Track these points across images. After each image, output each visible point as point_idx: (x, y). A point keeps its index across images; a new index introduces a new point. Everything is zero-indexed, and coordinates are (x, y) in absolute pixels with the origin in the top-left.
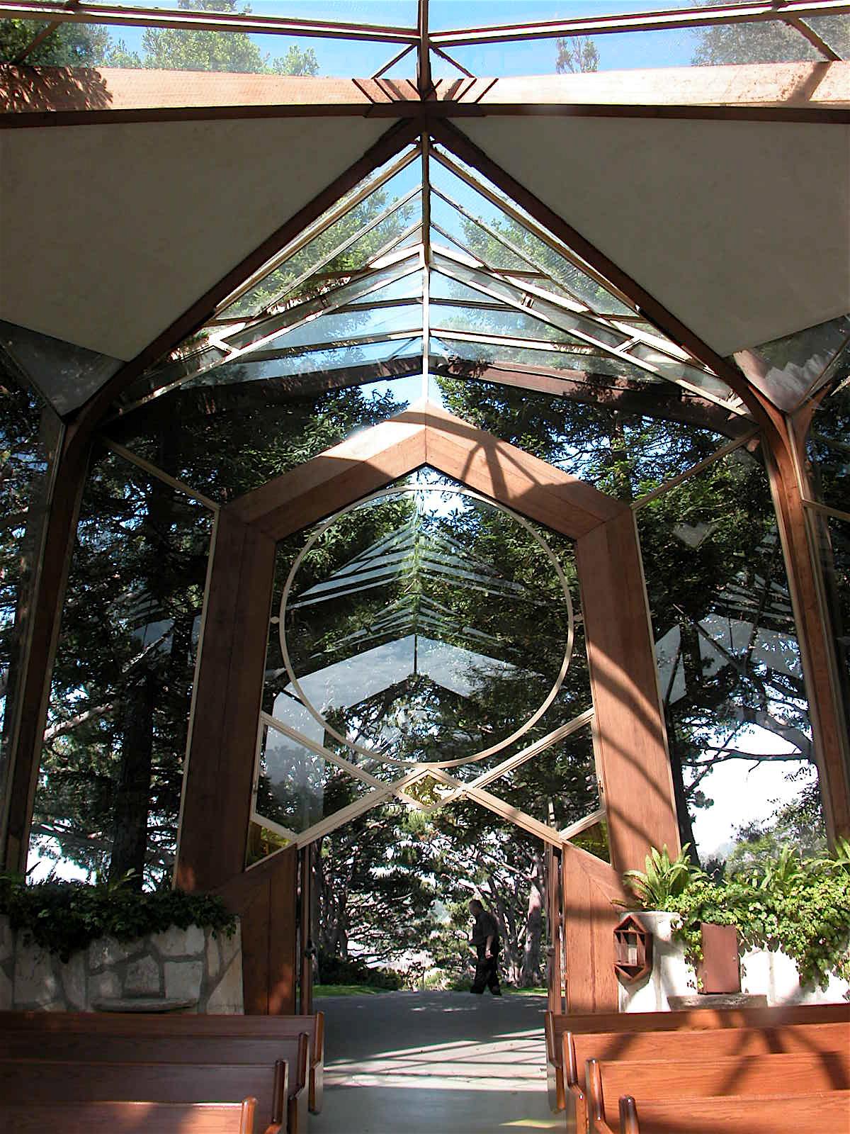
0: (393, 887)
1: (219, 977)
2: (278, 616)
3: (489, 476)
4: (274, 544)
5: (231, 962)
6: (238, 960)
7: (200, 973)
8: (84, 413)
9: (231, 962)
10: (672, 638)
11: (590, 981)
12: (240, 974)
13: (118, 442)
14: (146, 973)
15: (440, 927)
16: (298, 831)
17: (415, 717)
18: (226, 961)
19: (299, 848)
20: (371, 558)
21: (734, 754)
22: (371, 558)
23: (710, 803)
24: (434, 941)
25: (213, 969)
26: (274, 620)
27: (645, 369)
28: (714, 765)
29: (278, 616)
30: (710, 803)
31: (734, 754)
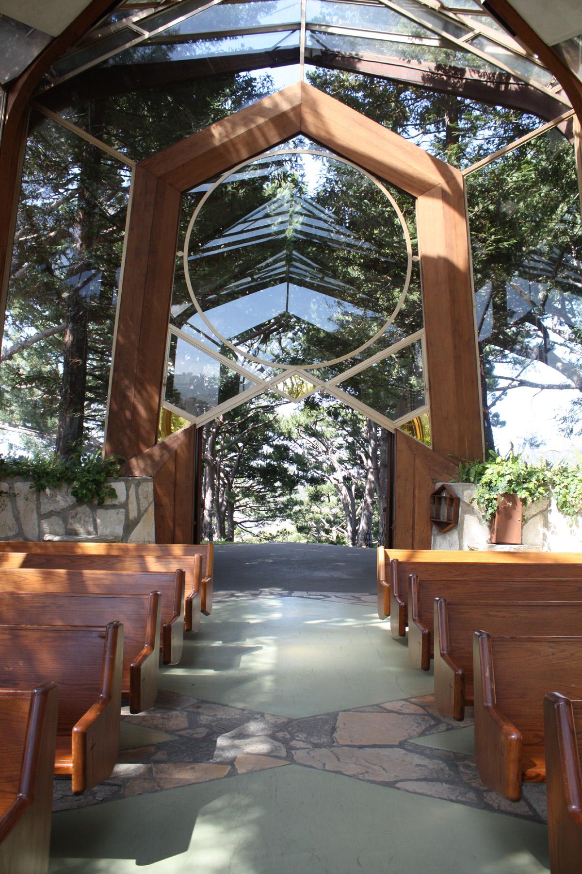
0: (270, 475)
1: (136, 522)
2: (183, 251)
3: (336, 6)
4: (179, 194)
5: (146, 510)
6: (152, 509)
7: (123, 517)
8: (21, 83)
9: (146, 510)
10: (485, 291)
11: (411, 531)
12: (153, 518)
13: (52, 110)
14: (83, 517)
15: (301, 503)
16: (197, 415)
17: (289, 342)
18: (142, 509)
19: (198, 427)
20: (257, 220)
21: (522, 383)
22: (257, 220)
23: (503, 424)
24: (296, 513)
25: (133, 514)
26: (179, 254)
27: (478, 56)
28: (508, 391)
29: (183, 251)
30: (503, 424)
31: (522, 383)
